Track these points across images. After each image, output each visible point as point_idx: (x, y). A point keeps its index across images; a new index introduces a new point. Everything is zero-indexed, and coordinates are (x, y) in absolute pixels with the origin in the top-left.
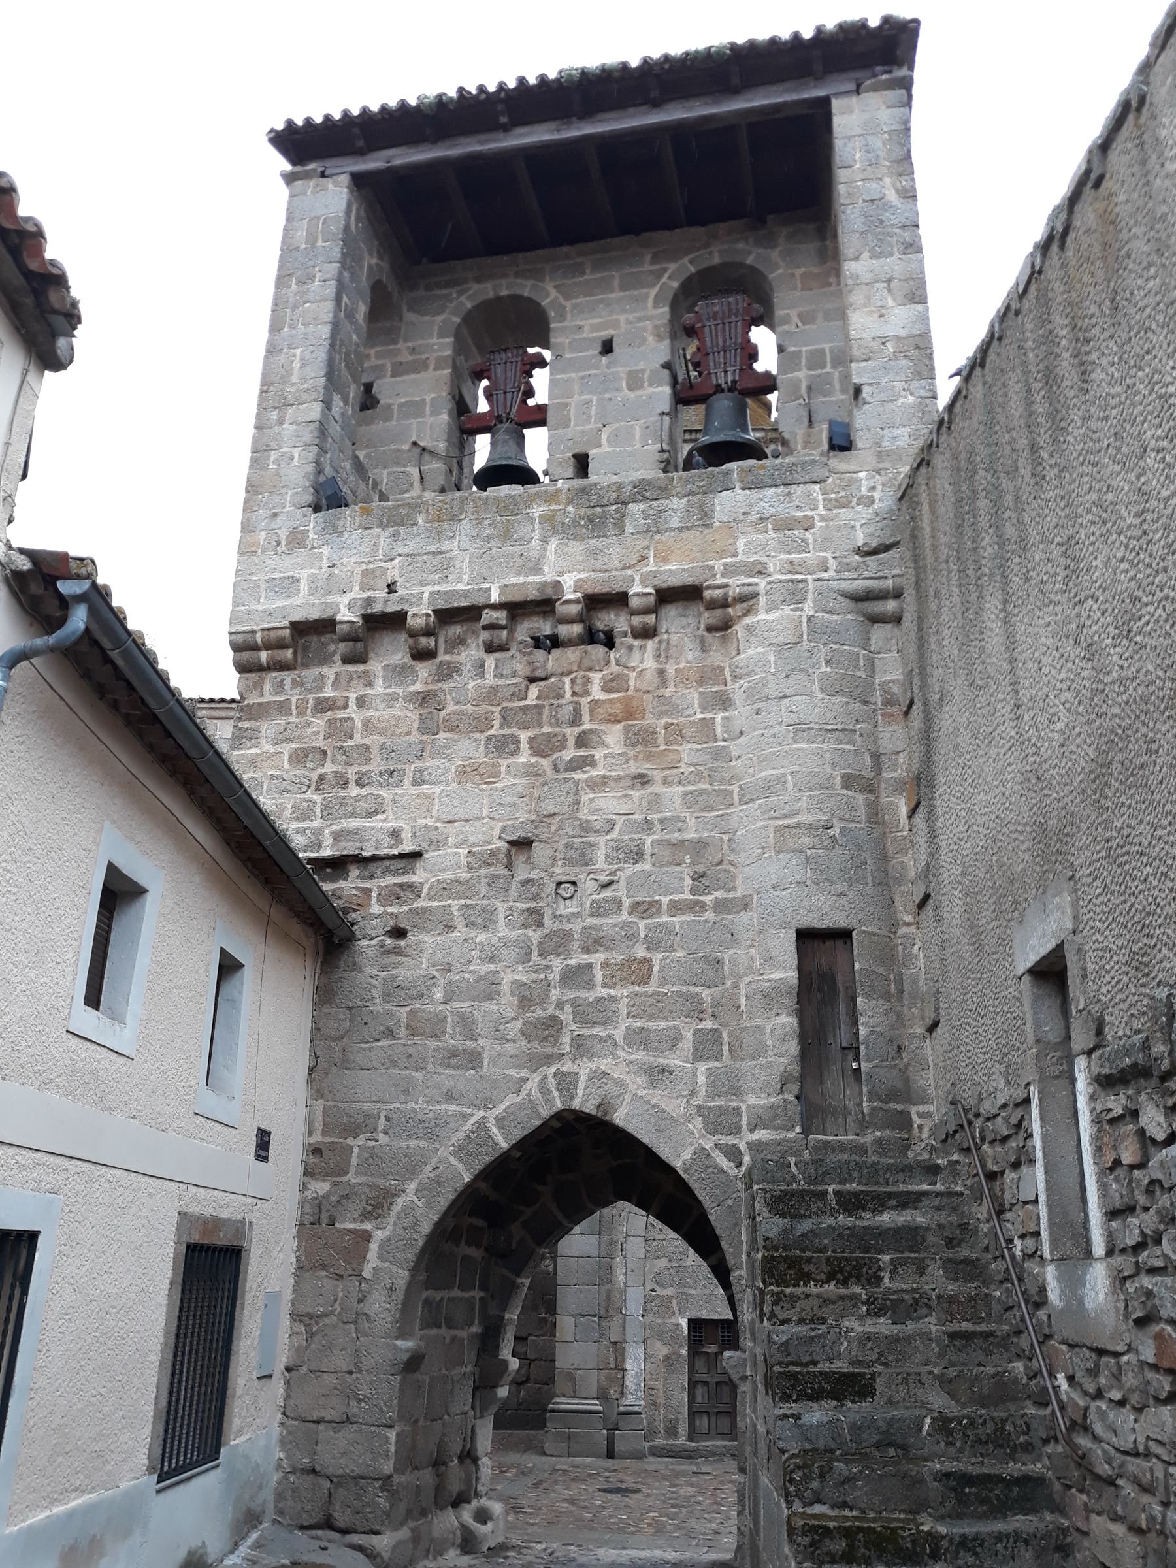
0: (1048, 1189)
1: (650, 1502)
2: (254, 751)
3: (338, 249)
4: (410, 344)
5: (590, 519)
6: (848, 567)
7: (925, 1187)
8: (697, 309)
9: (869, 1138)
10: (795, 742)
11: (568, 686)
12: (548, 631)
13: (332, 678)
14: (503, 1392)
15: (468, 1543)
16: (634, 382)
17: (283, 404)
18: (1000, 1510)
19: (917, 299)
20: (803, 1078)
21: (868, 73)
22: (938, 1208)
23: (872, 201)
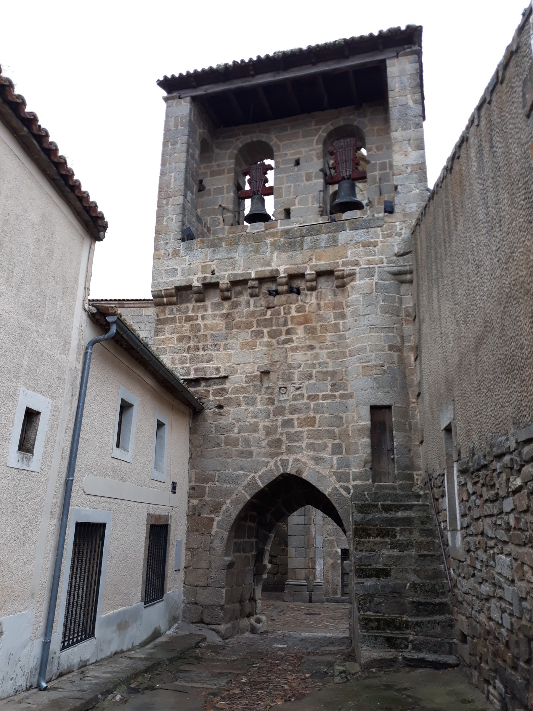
0: (449, 506)
1: (324, 618)
2: (163, 337)
3: (187, 130)
4: (217, 163)
5: (290, 244)
6: (391, 262)
7: (416, 503)
8: (334, 144)
9: (397, 484)
10: (370, 333)
11: (282, 310)
12: (274, 288)
13: (192, 308)
14: (265, 576)
15: (253, 630)
16: (309, 178)
17: (168, 197)
18: (431, 614)
19: (420, 148)
20: (372, 462)
21: (401, 48)
22: (419, 510)
23: (403, 105)
